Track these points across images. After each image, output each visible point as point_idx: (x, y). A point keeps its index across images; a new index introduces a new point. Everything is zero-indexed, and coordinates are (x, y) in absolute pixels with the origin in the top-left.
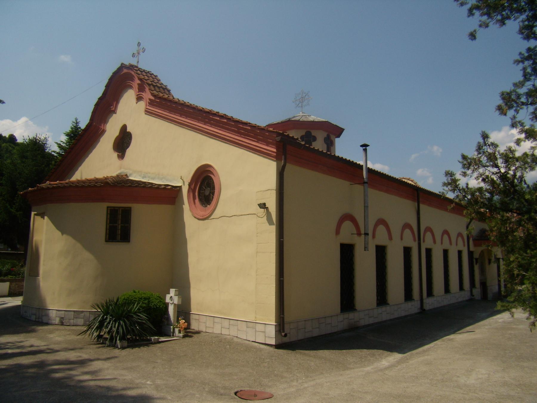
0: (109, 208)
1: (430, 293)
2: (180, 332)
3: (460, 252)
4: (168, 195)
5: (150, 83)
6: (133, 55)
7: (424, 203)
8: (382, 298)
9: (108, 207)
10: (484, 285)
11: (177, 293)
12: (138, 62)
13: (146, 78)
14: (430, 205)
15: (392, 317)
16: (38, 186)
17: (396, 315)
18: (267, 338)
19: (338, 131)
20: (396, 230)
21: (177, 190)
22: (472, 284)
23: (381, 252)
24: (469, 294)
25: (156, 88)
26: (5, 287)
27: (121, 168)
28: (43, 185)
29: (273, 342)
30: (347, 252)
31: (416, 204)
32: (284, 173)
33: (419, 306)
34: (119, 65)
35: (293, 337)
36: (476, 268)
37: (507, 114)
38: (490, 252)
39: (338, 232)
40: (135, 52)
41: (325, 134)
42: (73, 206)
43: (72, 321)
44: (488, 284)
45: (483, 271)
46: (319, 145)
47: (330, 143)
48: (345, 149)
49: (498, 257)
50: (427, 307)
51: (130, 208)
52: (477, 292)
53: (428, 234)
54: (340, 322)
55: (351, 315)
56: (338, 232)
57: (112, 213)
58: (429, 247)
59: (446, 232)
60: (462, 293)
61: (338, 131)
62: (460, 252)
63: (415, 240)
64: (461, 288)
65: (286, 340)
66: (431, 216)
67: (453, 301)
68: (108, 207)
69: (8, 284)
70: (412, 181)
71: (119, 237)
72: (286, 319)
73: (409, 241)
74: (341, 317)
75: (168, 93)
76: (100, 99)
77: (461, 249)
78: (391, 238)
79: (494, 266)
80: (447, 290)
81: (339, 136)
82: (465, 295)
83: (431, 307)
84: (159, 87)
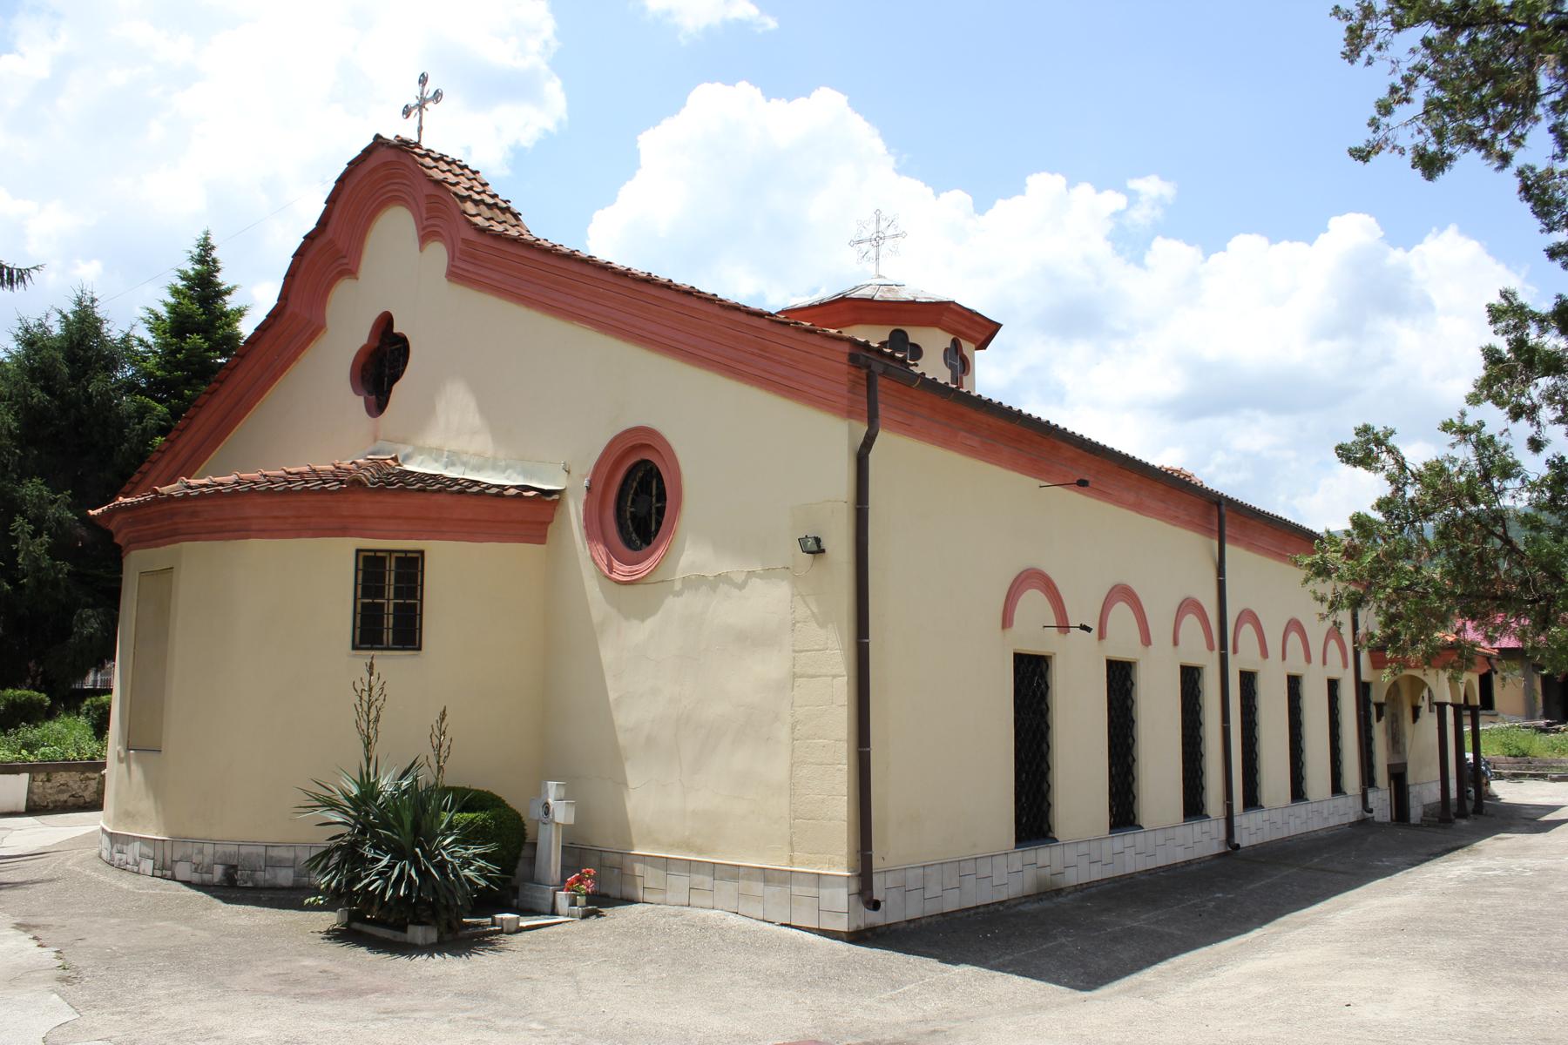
0: (362, 554)
2: (573, 903)
3: (1333, 685)
4: (523, 515)
5: (466, 193)
6: (407, 112)
7: (1236, 541)
8: (1123, 813)
9: (358, 551)
10: (1398, 777)
11: (562, 793)
12: (420, 129)
13: (452, 179)
14: (1250, 546)
15: (1151, 864)
16: (156, 492)
17: (1161, 860)
18: (824, 916)
19: (983, 330)
20: (1160, 620)
21: (548, 500)
22: (1368, 780)
23: (1120, 676)
24: (1359, 807)
25: (483, 207)
26: (15, 788)
27: (375, 440)
28: (173, 489)
29: (842, 925)
30: (1031, 676)
31: (1216, 543)
32: (871, 456)
33: (1223, 836)
34: (369, 141)
35: (893, 913)
36: (1379, 731)
37: (1387, 90)
38: (1418, 685)
39: (1007, 621)
40: (414, 102)
41: (945, 340)
42: (256, 548)
43: (260, 875)
44: (1410, 780)
45: (1396, 740)
46: (933, 366)
47: (961, 365)
48: (991, 375)
49: (1437, 699)
50: (1244, 839)
51: (422, 553)
52: (1381, 799)
53: (1248, 630)
54: (1014, 874)
55: (1042, 855)
56: (1007, 621)
57: (370, 568)
58: (1248, 667)
59: (1295, 625)
60: (1340, 800)
61: (983, 330)
62: (1333, 685)
63: (1211, 648)
64: (1337, 788)
65: (876, 918)
67: (1316, 824)
68: (358, 551)
69: (25, 777)
71: (388, 636)
72: (877, 864)
75: (514, 222)
76: (309, 238)
77: (1334, 676)
78: (1146, 640)
79: (1429, 721)
80: (1298, 793)
81: (983, 345)
82: (1346, 810)
83: (1254, 840)
84: (490, 206)
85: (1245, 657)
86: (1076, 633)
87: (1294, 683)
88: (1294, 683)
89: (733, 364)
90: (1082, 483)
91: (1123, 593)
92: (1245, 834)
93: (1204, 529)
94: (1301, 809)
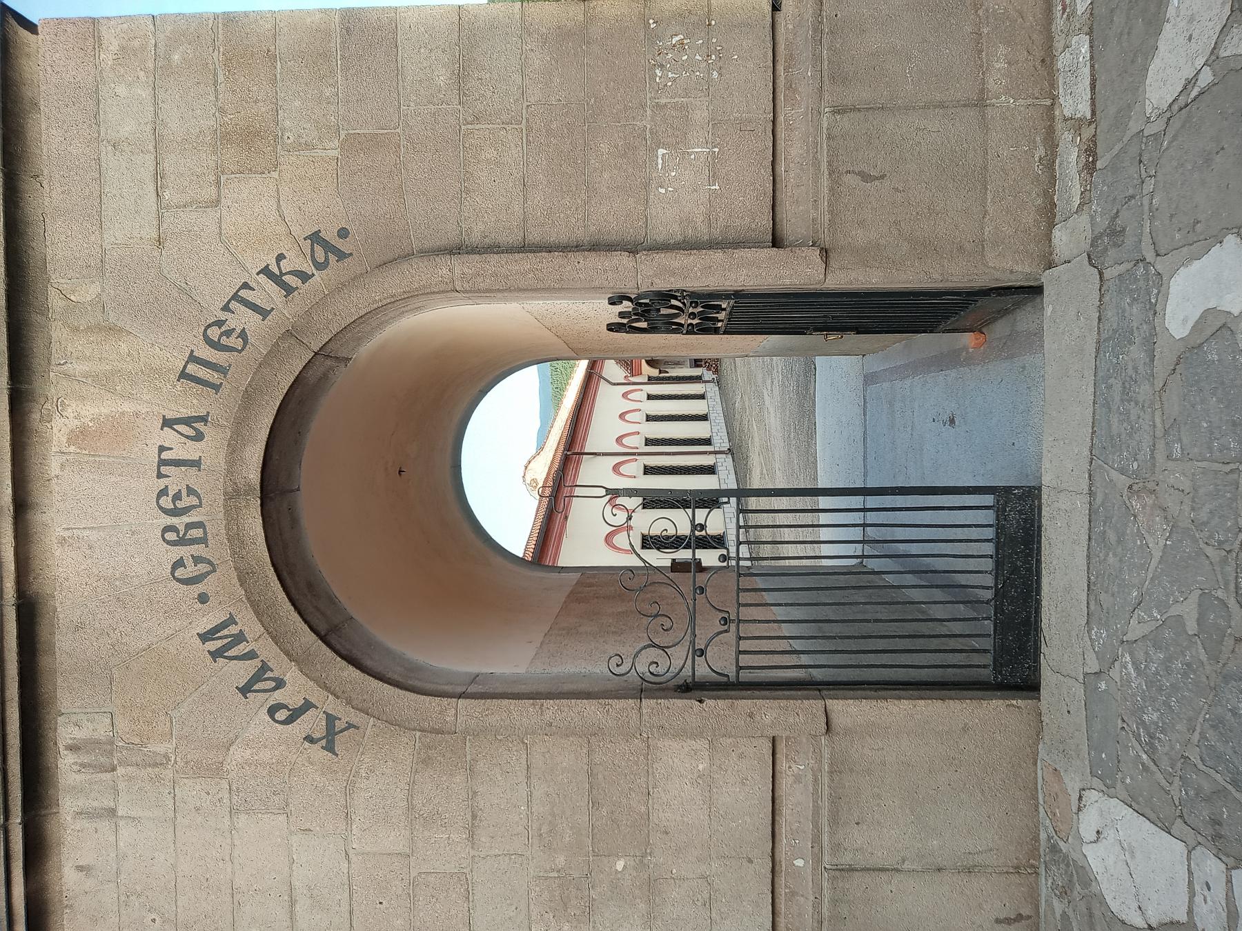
3: (650, 397)
36: (674, 372)
60: (709, 395)
64: (702, 397)
80: (704, 418)
82: (712, 390)
85: (636, 442)
86: (632, 523)
87: (649, 418)
88: (649, 418)
90: (310, 585)
93: (579, 463)
94: (712, 416)
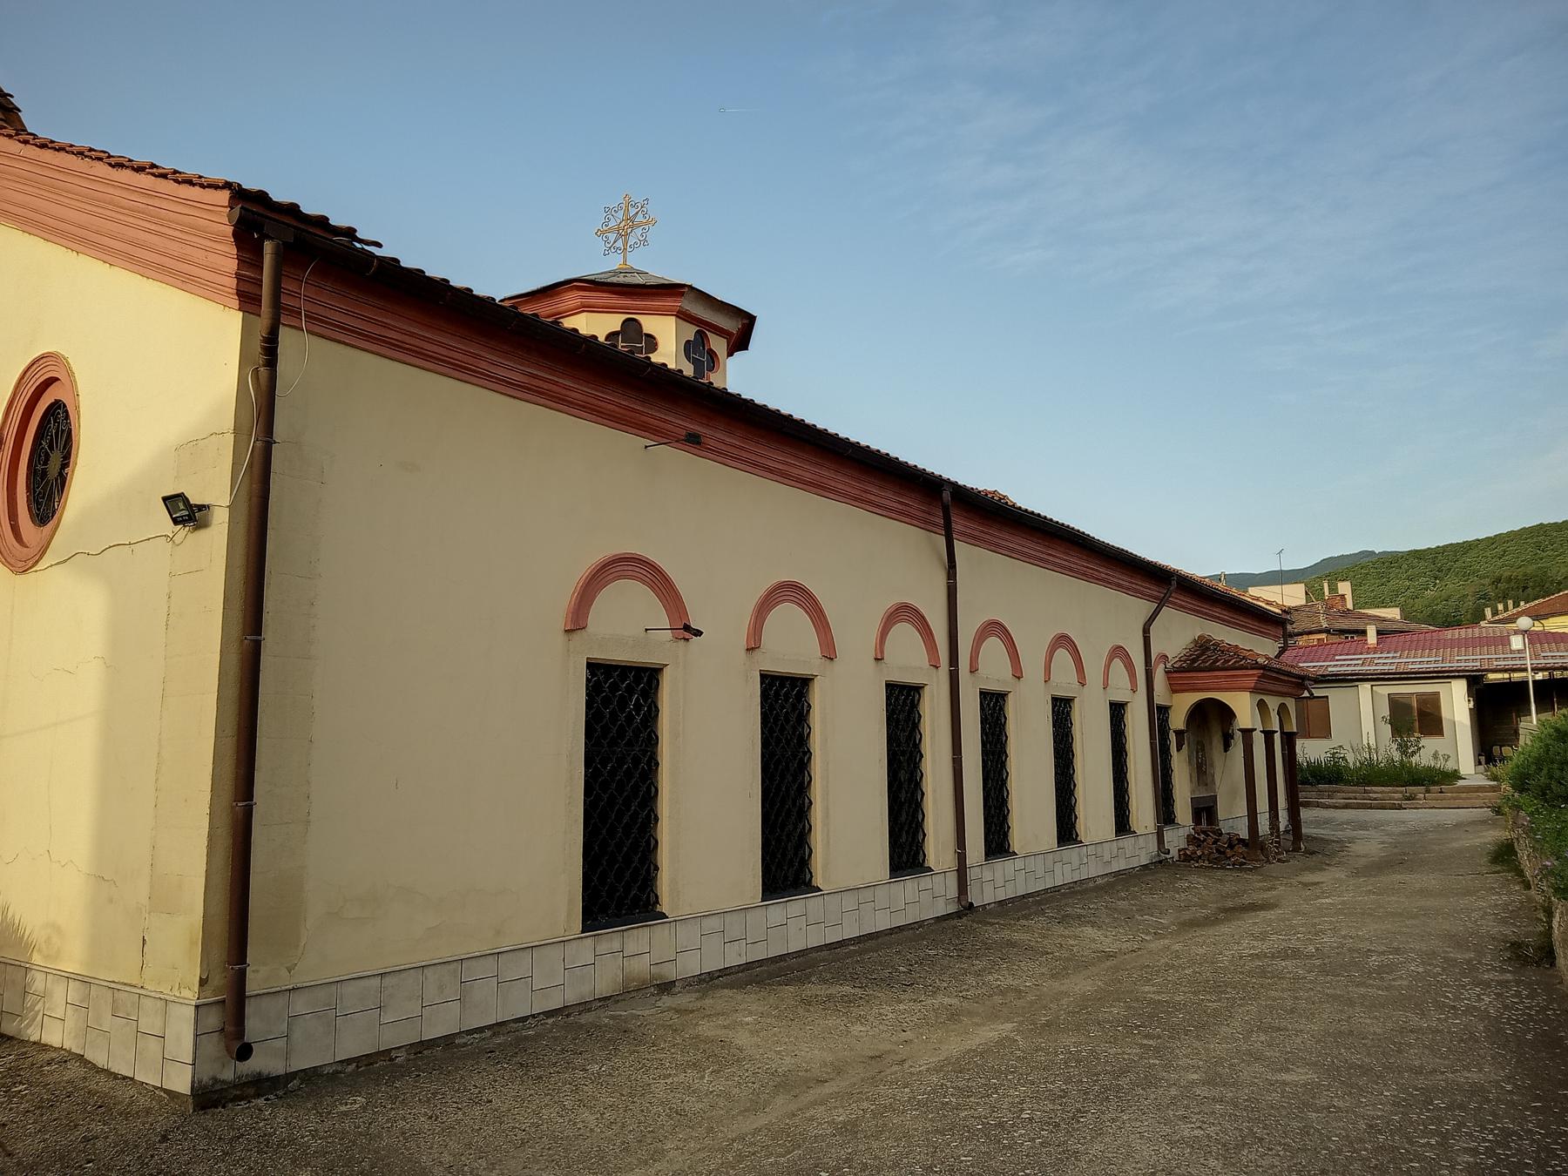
1: (998, 845)
3: (1117, 711)
7: (974, 540)
10: (1205, 810)
22: (1165, 814)
30: (621, 707)
31: (942, 541)
33: (953, 891)
39: (577, 623)
48: (740, 376)
50: (975, 898)
53: (994, 645)
56: (577, 623)
62: (1117, 711)
64: (1123, 825)
66: (996, 582)
67: (1094, 870)
70: (1305, 885)
73: (909, 658)
74: (585, 949)
77: (1119, 697)
78: (1018, 676)
80: (1067, 832)
82: (1139, 850)
89: (139, 253)
91: (1063, 641)
92: (988, 889)
93: (926, 525)
94: (1071, 853)
